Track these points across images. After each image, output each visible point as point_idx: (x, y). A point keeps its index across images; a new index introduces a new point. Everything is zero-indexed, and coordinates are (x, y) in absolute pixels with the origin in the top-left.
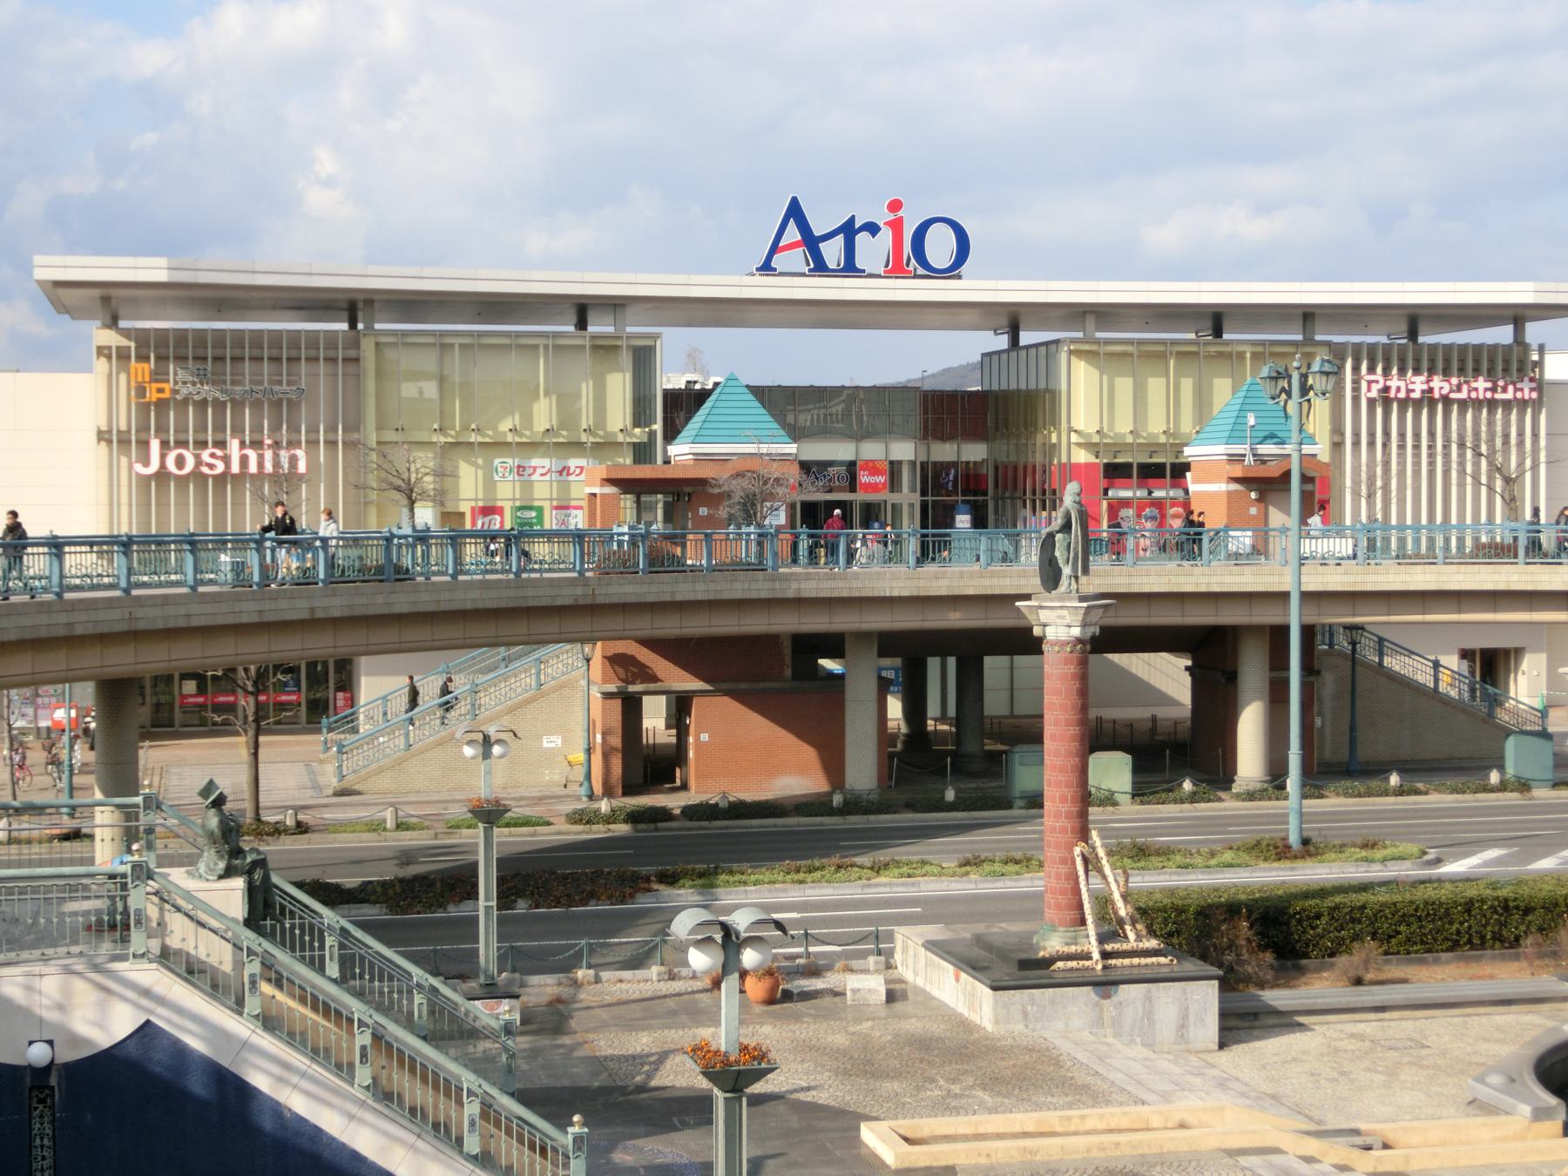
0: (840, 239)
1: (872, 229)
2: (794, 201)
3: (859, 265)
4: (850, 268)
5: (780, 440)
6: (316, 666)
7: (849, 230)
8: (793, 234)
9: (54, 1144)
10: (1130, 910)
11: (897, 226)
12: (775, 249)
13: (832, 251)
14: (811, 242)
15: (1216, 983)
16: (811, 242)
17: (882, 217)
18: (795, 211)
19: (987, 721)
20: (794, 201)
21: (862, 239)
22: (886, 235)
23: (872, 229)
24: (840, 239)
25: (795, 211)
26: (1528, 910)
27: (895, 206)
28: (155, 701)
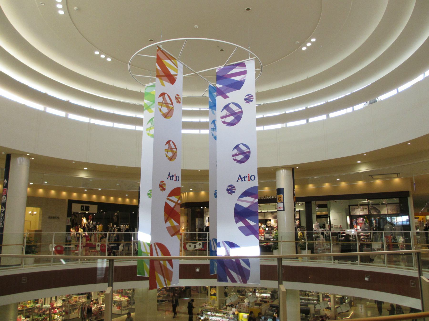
0: (244, 178)
1: (247, 177)
2: (240, 175)
3: (246, 180)
4: (245, 180)
5: (380, 265)
6: (415, 248)
7: (245, 177)
8: (240, 178)
9: (214, 320)
10: (248, 295)
11: (249, 176)
12: (238, 179)
13: (243, 179)
14: (241, 179)
15: (272, 319)
16: (241, 179)
17: (247, 176)
18: (240, 176)
19: (373, 249)
20: (240, 175)
21: (246, 178)
22: (248, 177)
23: (247, 177)
24: (244, 178)
25: (240, 176)
26: (343, 222)
27: (249, 174)
28: (125, 255)
